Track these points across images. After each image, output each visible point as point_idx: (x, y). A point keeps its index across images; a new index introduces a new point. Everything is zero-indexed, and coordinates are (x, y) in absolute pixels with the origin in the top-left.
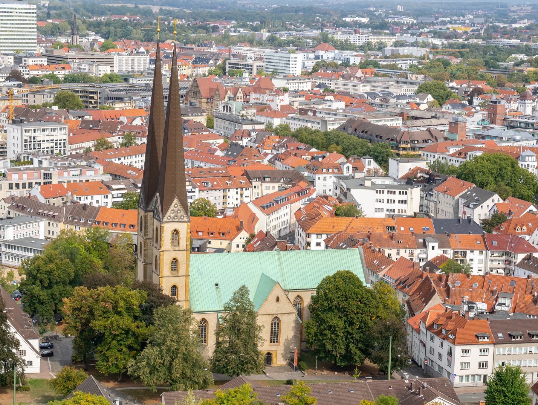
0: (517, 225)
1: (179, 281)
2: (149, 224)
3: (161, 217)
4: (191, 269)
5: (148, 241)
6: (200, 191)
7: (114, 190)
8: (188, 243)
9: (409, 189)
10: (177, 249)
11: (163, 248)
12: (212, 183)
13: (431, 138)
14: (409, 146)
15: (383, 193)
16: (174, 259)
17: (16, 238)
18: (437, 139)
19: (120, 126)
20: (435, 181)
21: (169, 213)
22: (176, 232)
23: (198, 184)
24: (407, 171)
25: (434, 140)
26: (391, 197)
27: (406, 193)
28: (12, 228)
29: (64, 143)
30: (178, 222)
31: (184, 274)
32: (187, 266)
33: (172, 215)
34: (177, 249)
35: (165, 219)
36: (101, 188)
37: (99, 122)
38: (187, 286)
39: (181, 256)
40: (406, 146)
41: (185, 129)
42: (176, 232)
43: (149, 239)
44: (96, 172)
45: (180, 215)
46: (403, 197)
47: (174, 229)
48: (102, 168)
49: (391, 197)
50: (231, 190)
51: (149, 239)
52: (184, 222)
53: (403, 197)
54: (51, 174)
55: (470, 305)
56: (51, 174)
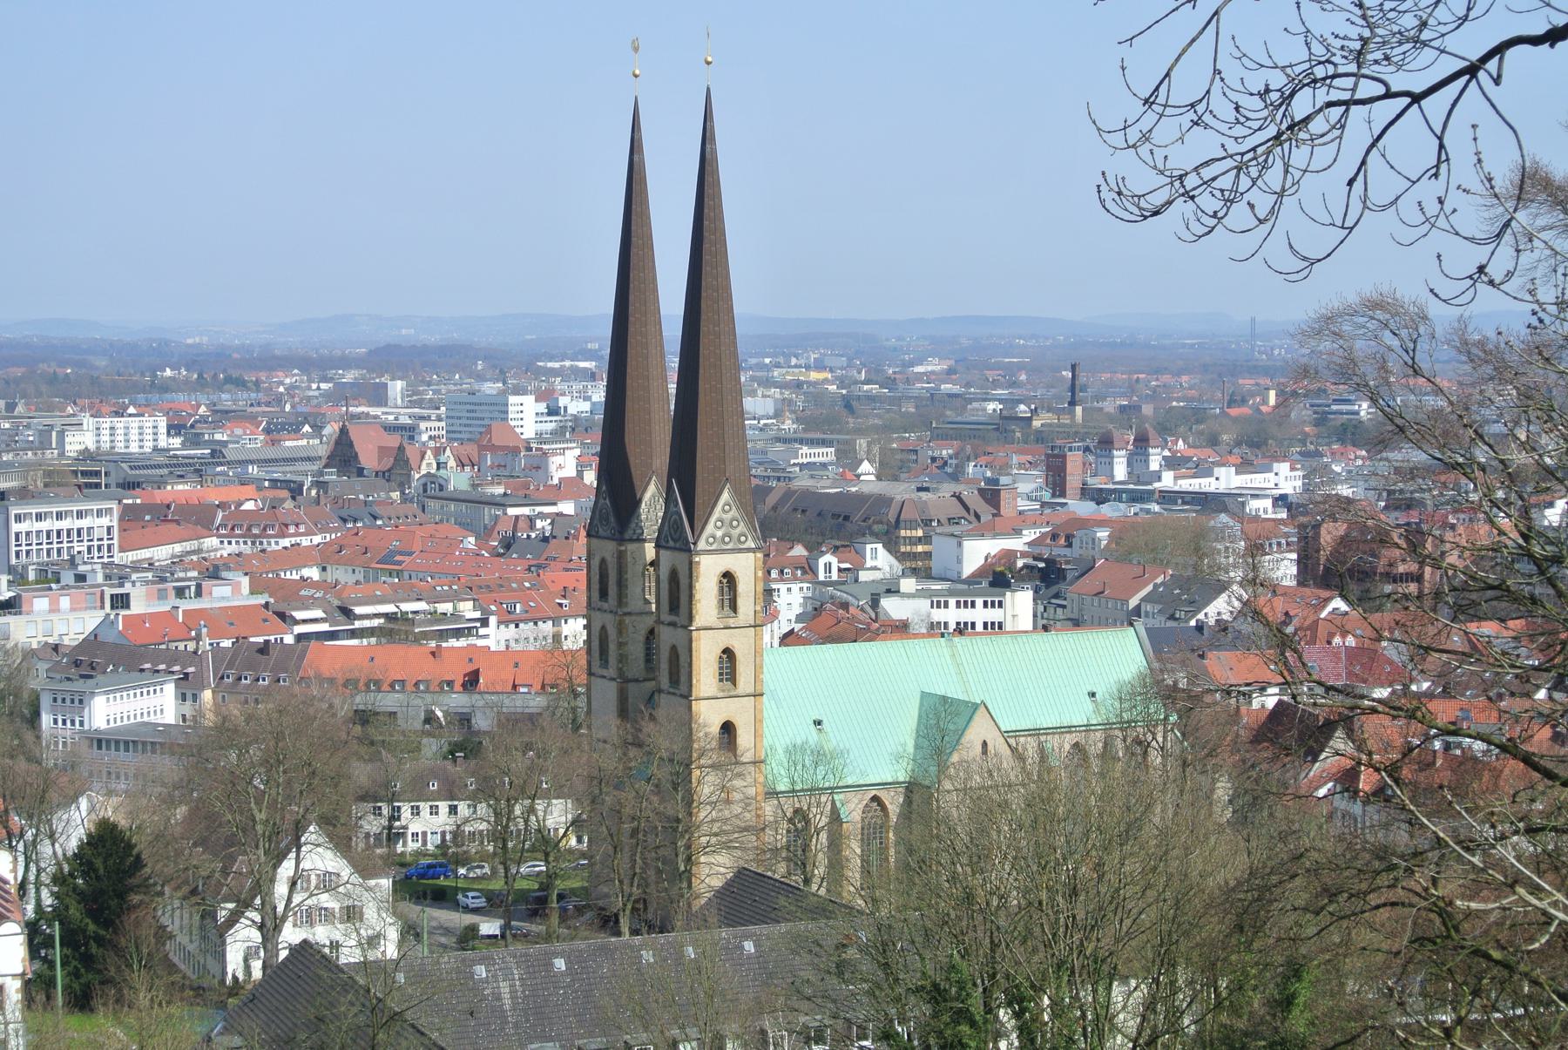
0: (1332, 635)
1: (738, 711)
2: (629, 576)
3: (691, 539)
4: (766, 676)
5: (627, 620)
6: (500, 623)
7: (297, 622)
8: (758, 608)
9: (1008, 594)
10: (731, 622)
11: (699, 621)
12: (525, 603)
13: (964, 513)
14: (920, 533)
15: (946, 606)
16: (724, 651)
17: (112, 724)
18: (978, 517)
19: (220, 515)
20: (1061, 575)
21: (710, 528)
22: (728, 579)
23: (493, 608)
24: (982, 562)
25: (972, 518)
26: (966, 615)
27: (1000, 604)
28: (104, 698)
29: (109, 547)
30: (733, 551)
31: (751, 690)
32: (758, 669)
33: (719, 534)
34: (731, 622)
35: (702, 545)
36: (265, 620)
37: (168, 506)
38: (758, 721)
39: (741, 643)
40: (914, 533)
41: (375, 518)
42: (728, 579)
43: (629, 614)
44: (236, 588)
45: (738, 531)
46: (994, 615)
47: (723, 569)
48: (245, 581)
49: (966, 615)
50: (571, 621)
51: (629, 614)
52: (749, 550)
53: (994, 615)
54: (128, 595)
55: (1451, 739)
56: (128, 595)
